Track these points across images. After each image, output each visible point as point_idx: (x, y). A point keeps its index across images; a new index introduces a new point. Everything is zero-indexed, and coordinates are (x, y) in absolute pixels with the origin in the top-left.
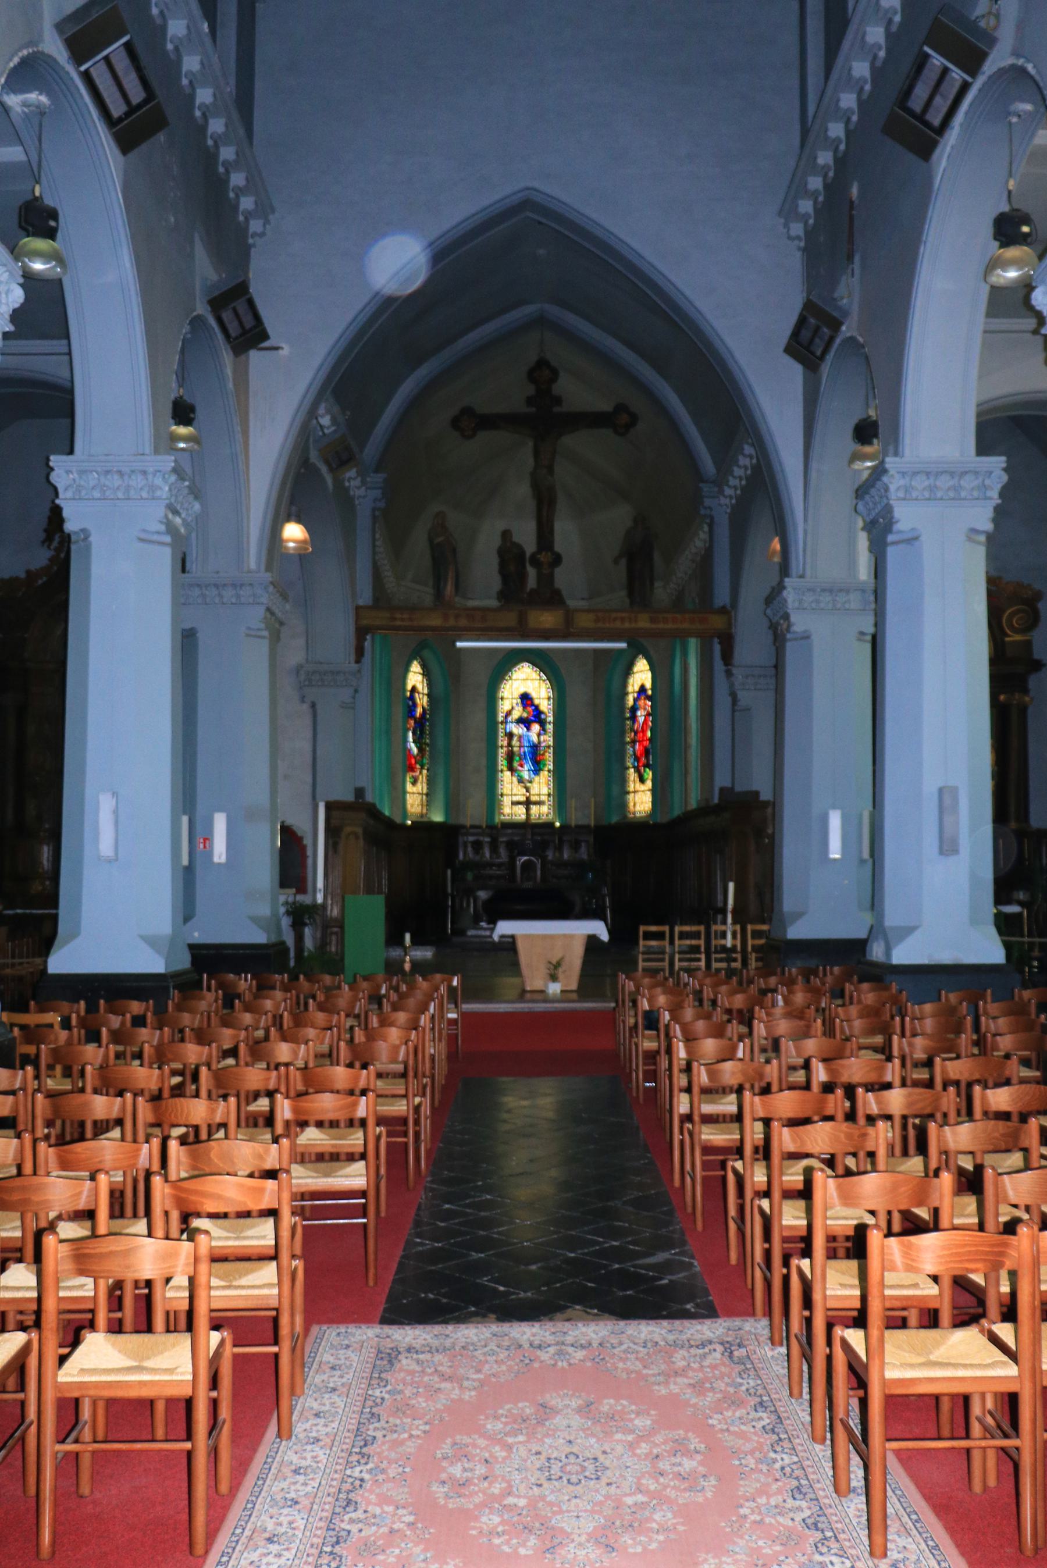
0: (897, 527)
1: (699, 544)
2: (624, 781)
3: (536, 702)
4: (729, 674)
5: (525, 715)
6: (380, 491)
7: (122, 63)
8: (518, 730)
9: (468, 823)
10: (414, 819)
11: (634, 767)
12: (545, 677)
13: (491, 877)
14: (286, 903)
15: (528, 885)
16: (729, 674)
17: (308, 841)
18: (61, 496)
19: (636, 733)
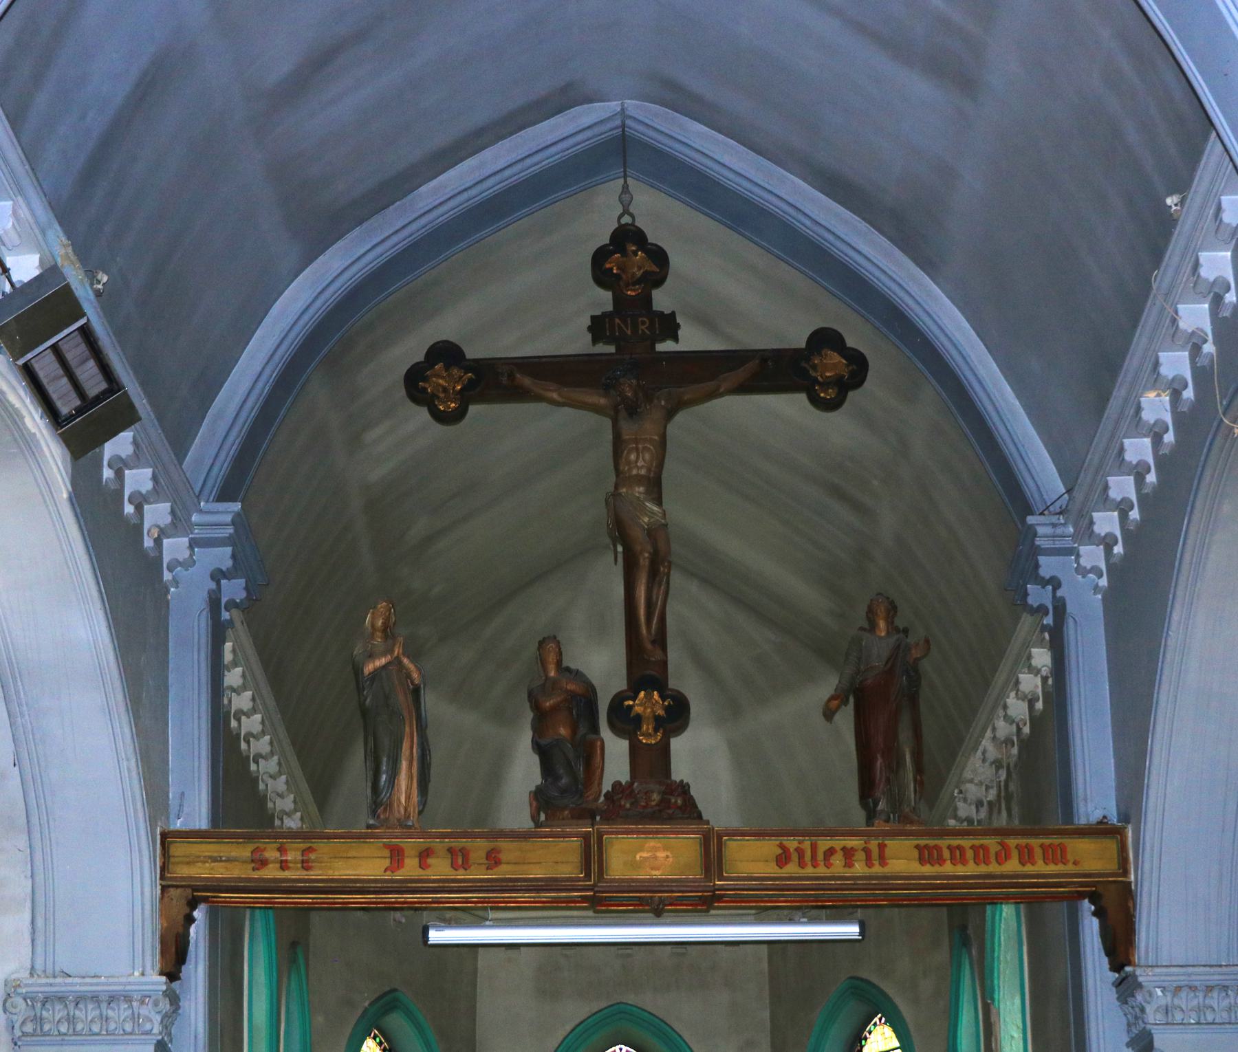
4: (1126, 987)
7: (75, 351)
16: (1126, 987)
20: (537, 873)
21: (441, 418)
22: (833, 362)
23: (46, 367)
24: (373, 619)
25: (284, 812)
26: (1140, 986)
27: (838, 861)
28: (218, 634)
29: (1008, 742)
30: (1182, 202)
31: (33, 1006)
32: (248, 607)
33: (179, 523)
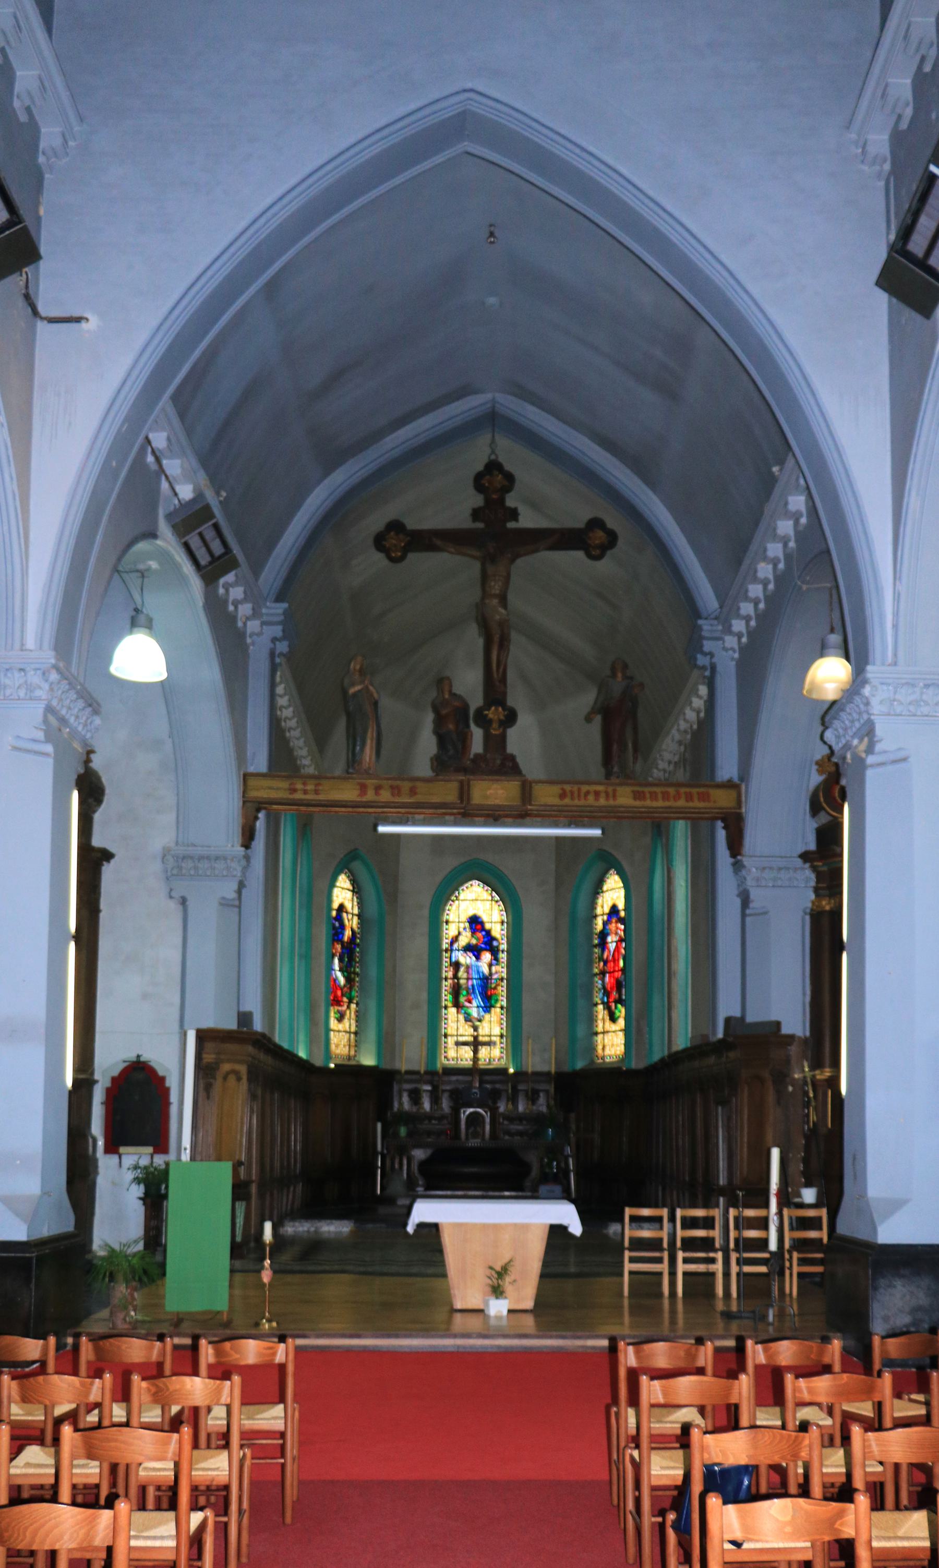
0: (751, 905)
1: (691, 715)
2: (591, 1019)
3: (487, 926)
4: (738, 866)
5: (474, 942)
6: (280, 628)
7: (210, 534)
8: (466, 959)
9: (404, 1068)
10: (339, 1062)
11: (603, 1003)
12: (497, 898)
13: (429, 1133)
14: (136, 1167)
15: (474, 1143)
16: (738, 866)
17: (172, 1083)
19: (606, 962)
20: (436, 799)
21: (392, 560)
22: (599, 536)
23: (195, 542)
24: (355, 665)
25: (302, 757)
26: (744, 867)
27: (591, 798)
28: (274, 668)
29: (685, 732)
30: (781, 470)
31: (177, 861)
32: (289, 657)
33: (256, 614)
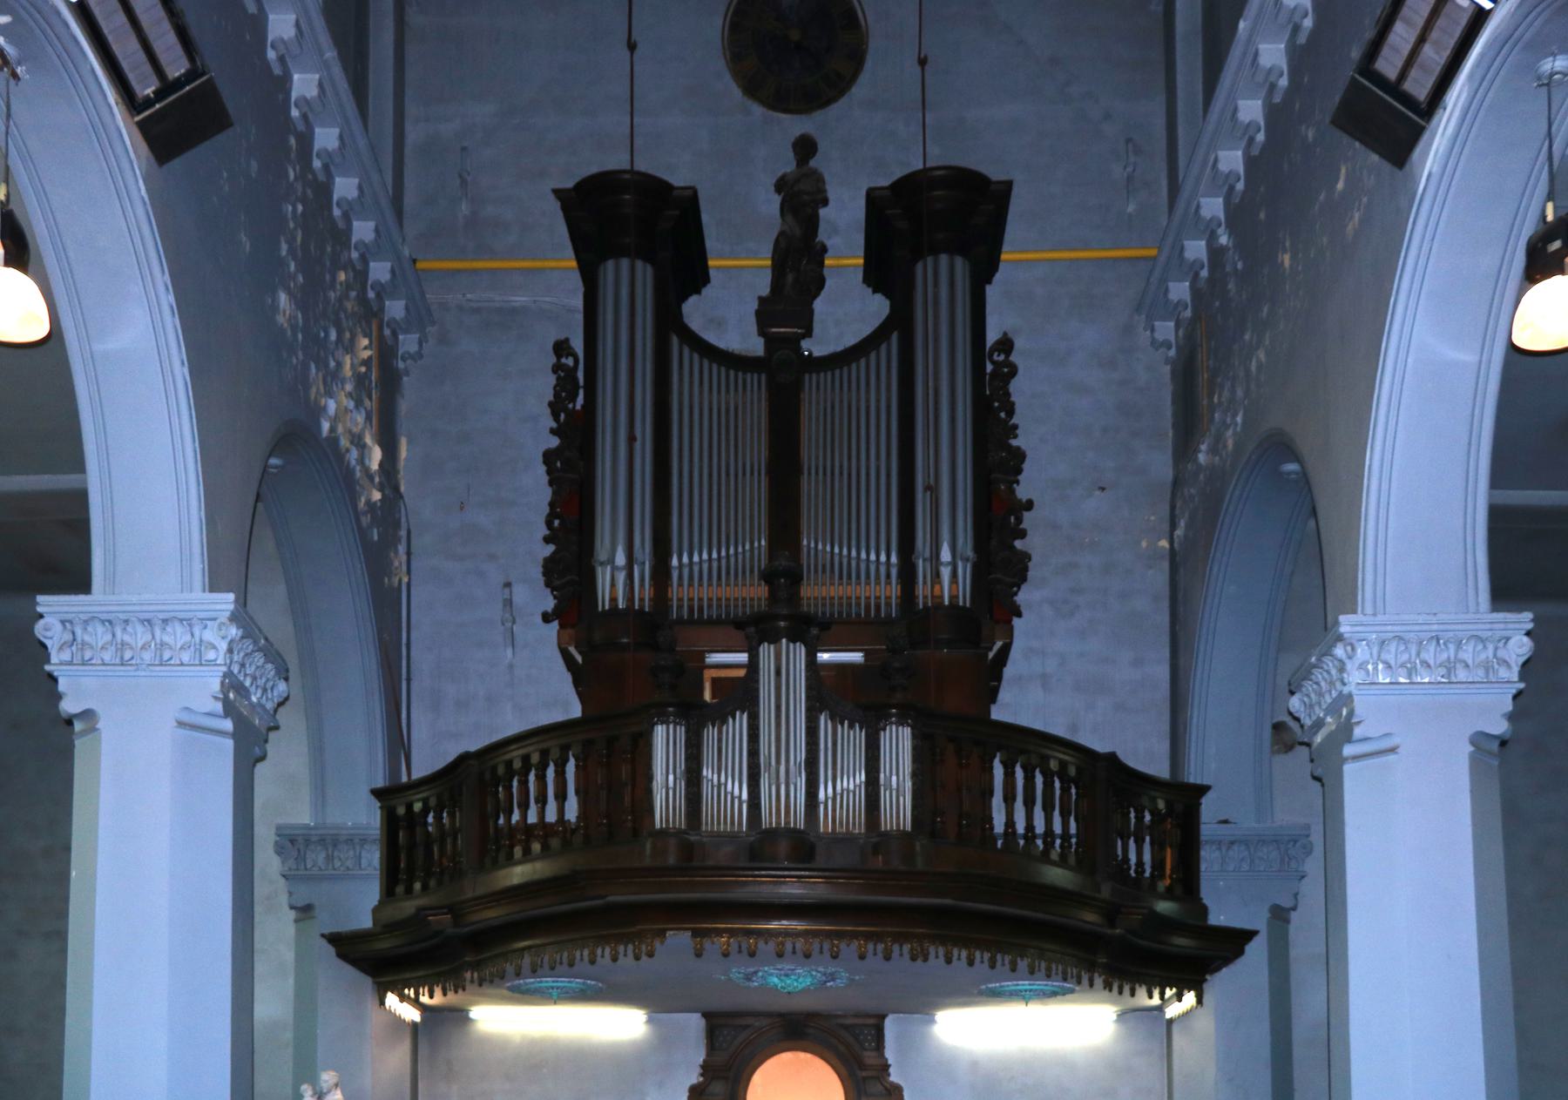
18: (54, 659)
